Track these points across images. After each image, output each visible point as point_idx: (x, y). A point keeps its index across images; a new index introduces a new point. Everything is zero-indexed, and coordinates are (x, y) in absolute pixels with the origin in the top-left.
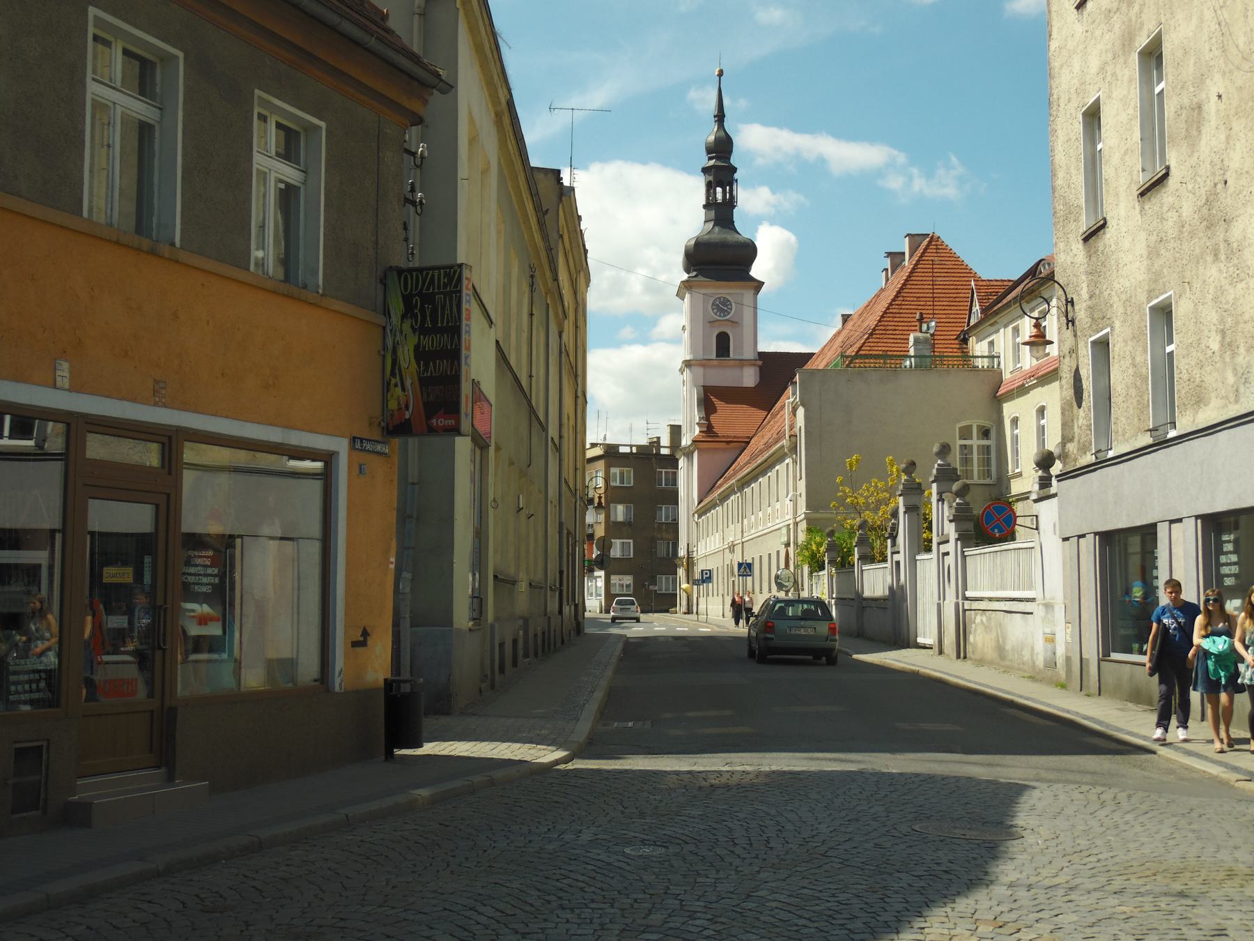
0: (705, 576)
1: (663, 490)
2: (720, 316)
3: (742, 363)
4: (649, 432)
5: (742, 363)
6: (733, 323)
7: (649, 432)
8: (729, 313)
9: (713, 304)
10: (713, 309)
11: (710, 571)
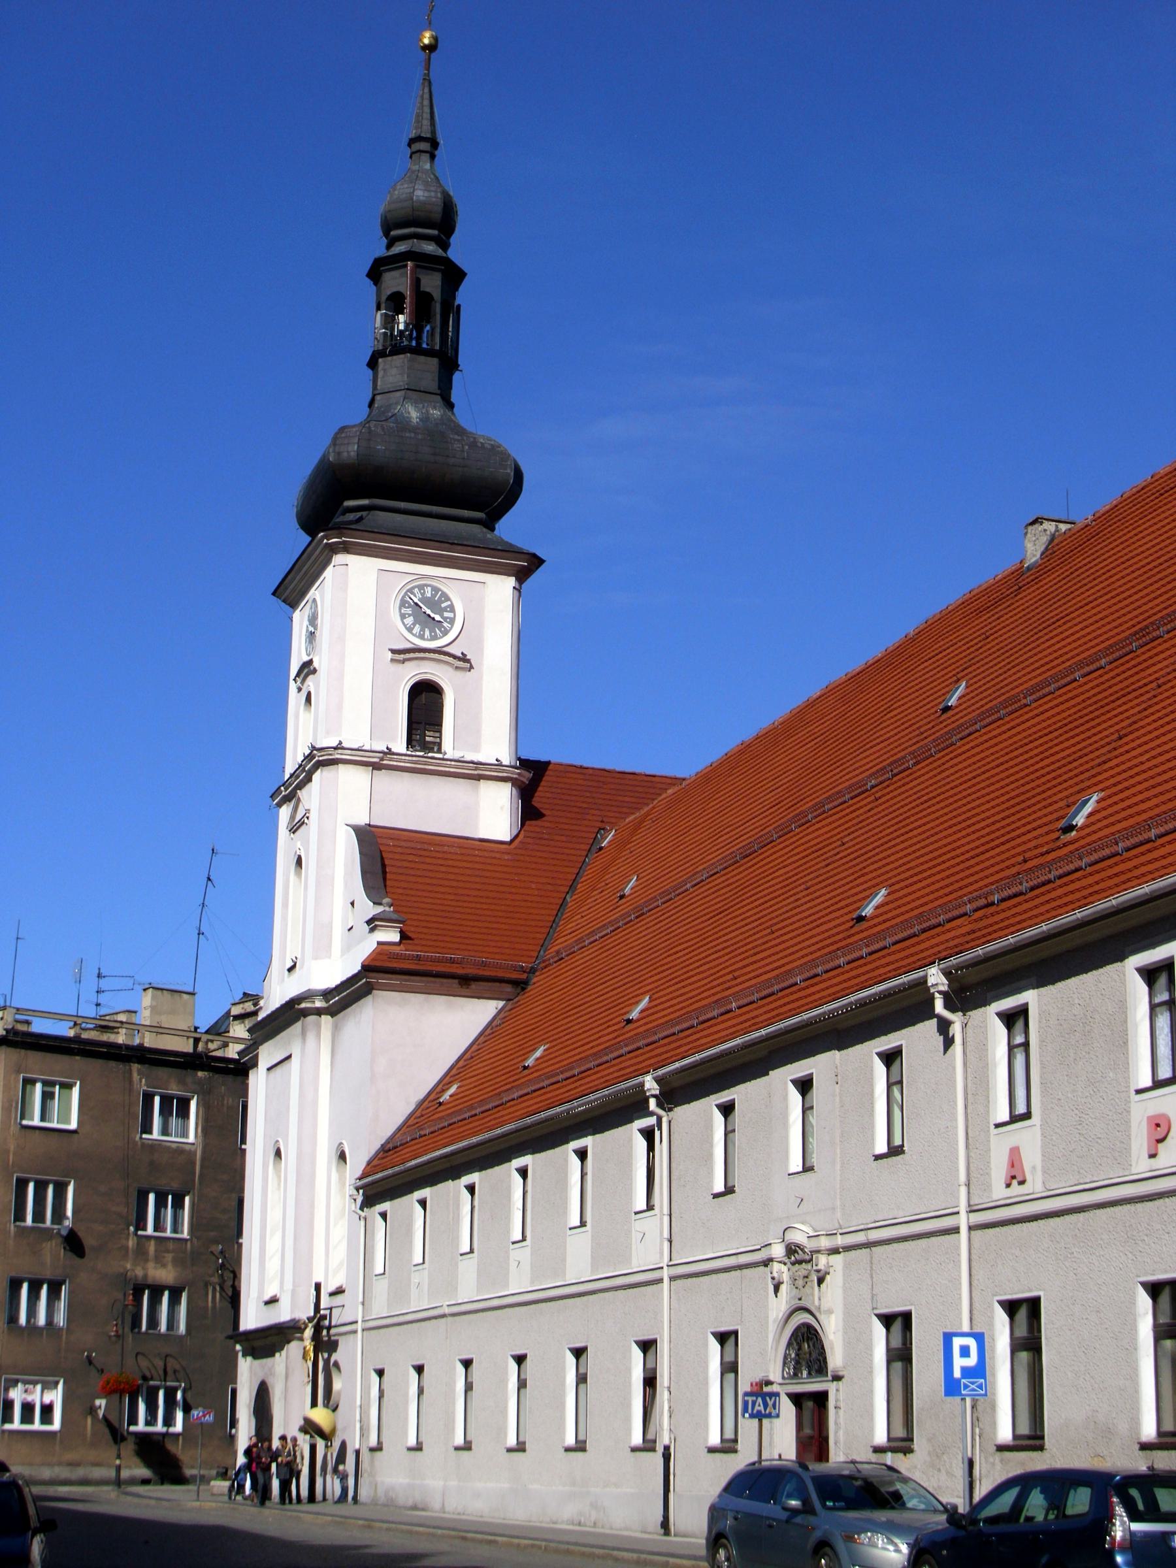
0: (959, 1363)
1: (155, 1146)
2: (422, 637)
3: (476, 773)
4: (103, 998)
5: (476, 773)
6: (464, 662)
7: (103, 998)
8: (446, 633)
9: (403, 603)
10: (403, 617)
11: (986, 1395)
